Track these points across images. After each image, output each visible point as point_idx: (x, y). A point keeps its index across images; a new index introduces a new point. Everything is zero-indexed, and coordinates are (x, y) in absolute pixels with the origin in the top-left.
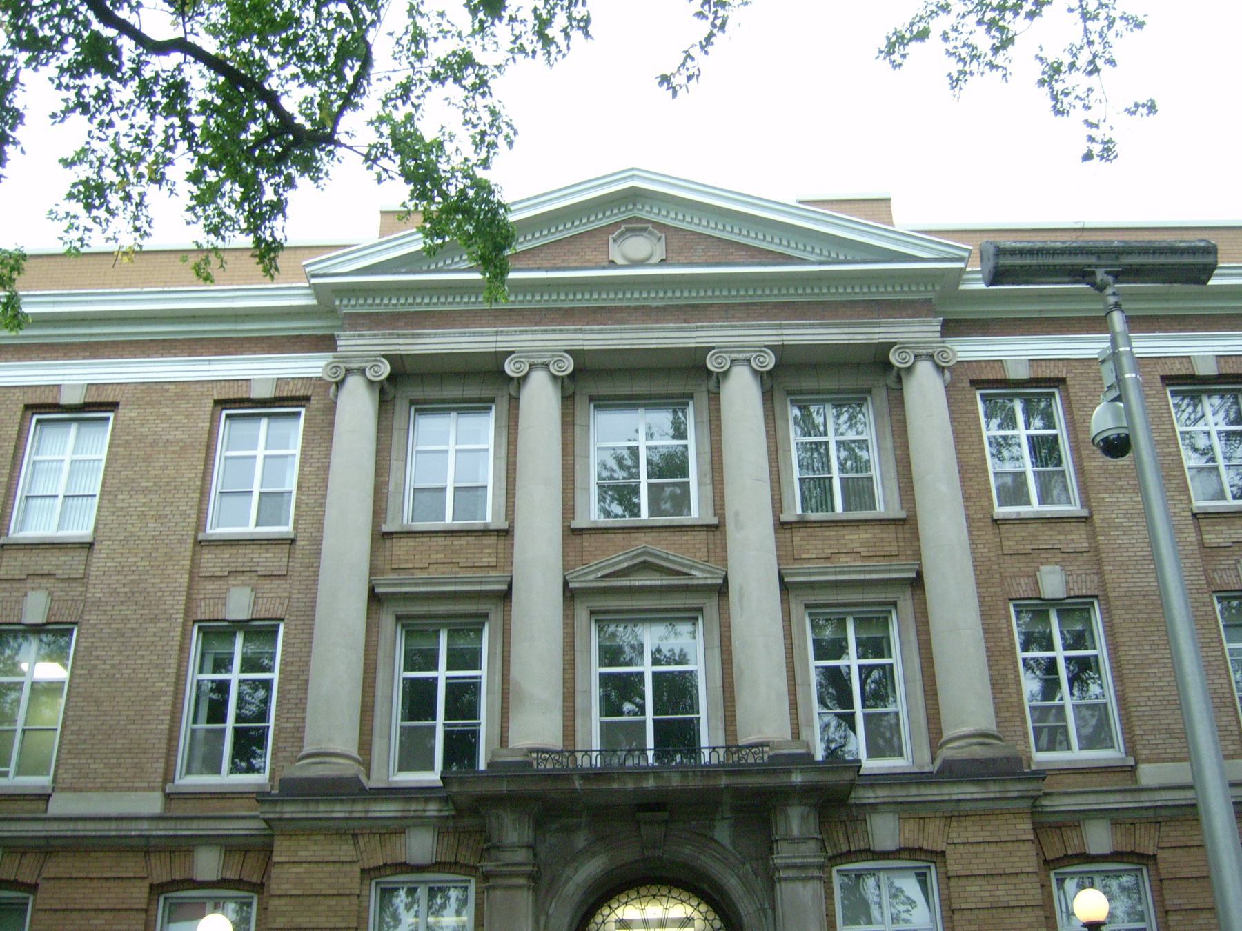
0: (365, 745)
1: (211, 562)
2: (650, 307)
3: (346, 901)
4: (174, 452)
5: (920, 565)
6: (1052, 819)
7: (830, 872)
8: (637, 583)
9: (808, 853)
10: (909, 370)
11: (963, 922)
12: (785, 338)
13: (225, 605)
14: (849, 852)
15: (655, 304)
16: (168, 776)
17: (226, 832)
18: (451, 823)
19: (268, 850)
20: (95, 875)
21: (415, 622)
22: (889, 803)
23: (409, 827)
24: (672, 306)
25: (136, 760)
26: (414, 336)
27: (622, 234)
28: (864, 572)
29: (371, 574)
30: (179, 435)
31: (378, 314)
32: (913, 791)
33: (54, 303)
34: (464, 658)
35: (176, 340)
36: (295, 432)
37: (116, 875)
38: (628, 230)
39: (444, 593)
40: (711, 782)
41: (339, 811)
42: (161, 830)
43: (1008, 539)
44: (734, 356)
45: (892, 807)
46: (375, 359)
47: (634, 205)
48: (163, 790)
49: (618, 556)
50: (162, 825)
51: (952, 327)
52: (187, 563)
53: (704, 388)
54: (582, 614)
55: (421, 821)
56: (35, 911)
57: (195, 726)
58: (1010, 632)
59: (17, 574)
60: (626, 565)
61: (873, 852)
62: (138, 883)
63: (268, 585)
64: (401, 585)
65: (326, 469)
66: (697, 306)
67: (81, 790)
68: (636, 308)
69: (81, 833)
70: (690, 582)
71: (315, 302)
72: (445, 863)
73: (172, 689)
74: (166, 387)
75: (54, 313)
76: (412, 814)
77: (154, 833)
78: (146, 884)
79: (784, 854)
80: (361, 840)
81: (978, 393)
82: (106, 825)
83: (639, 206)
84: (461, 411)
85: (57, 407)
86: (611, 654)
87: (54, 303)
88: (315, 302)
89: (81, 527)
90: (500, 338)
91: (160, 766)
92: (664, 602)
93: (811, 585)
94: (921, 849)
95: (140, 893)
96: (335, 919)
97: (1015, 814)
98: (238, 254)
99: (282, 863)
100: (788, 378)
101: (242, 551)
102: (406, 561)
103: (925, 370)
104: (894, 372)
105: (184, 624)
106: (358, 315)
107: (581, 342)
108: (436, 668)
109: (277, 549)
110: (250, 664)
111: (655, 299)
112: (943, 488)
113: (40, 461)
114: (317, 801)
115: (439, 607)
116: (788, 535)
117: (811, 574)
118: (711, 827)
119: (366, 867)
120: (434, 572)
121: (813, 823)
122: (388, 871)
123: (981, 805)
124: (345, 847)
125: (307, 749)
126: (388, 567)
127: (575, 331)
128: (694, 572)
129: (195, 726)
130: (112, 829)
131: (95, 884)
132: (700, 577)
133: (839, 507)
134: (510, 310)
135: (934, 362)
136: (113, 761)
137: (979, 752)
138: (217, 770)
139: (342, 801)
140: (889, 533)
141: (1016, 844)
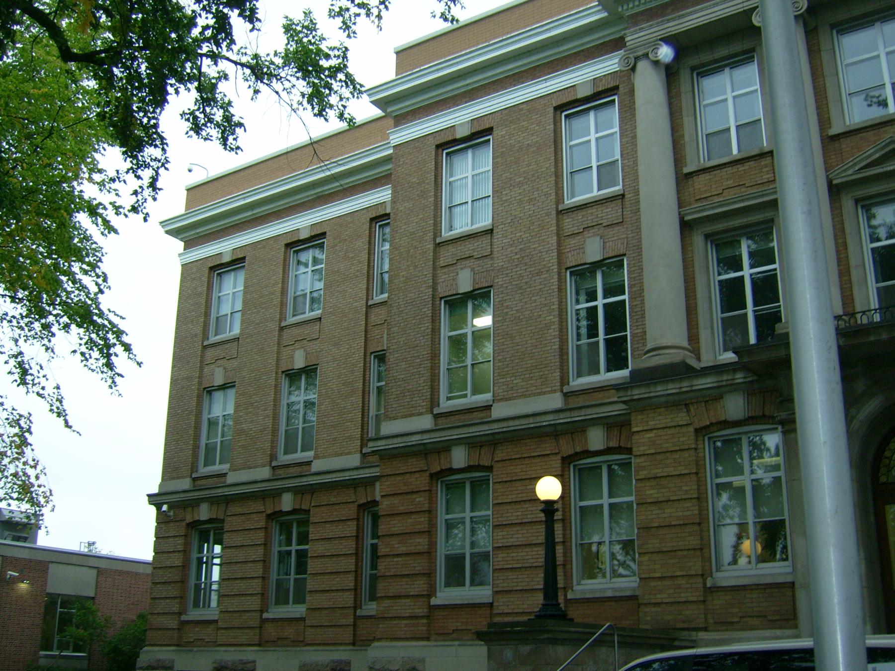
0: (693, 337)
1: (570, 224)
3: (686, 454)
4: (533, 152)
8: (889, 169)
16: (564, 381)
20: (525, 455)
21: (719, 237)
25: (541, 373)
26: (680, 17)
29: (680, 207)
30: (535, 138)
33: (438, 70)
34: (763, 256)
35: (522, 72)
36: (614, 113)
37: (539, 454)
41: (672, 388)
42: (562, 419)
48: (562, 391)
49: (871, 150)
50: (562, 415)
52: (554, 228)
54: (848, 203)
55: (734, 388)
56: (494, 483)
57: (579, 343)
59: (450, 261)
60: (877, 155)
62: (554, 457)
63: (610, 232)
64: (702, 211)
65: (634, 137)
67: (510, 399)
69: (512, 428)
71: (606, 14)
73: (557, 319)
74: (521, 107)
75: (439, 77)
76: (724, 383)
77: (558, 422)
78: (559, 457)
80: (691, 408)
82: (526, 421)
84: (733, 66)
85: (455, 142)
87: (438, 70)
88: (606, 14)
89: (485, 221)
91: (557, 374)
96: (680, 468)
99: (639, 432)
101: (590, 211)
105: (559, 273)
106: (637, 14)
109: (613, 205)
113: (455, 181)
114: (655, 384)
120: (727, 195)
124: (680, 415)
125: (649, 347)
129: (579, 343)
130: (530, 423)
131: (527, 461)
136: (527, 376)
138: (598, 372)
139: (672, 381)
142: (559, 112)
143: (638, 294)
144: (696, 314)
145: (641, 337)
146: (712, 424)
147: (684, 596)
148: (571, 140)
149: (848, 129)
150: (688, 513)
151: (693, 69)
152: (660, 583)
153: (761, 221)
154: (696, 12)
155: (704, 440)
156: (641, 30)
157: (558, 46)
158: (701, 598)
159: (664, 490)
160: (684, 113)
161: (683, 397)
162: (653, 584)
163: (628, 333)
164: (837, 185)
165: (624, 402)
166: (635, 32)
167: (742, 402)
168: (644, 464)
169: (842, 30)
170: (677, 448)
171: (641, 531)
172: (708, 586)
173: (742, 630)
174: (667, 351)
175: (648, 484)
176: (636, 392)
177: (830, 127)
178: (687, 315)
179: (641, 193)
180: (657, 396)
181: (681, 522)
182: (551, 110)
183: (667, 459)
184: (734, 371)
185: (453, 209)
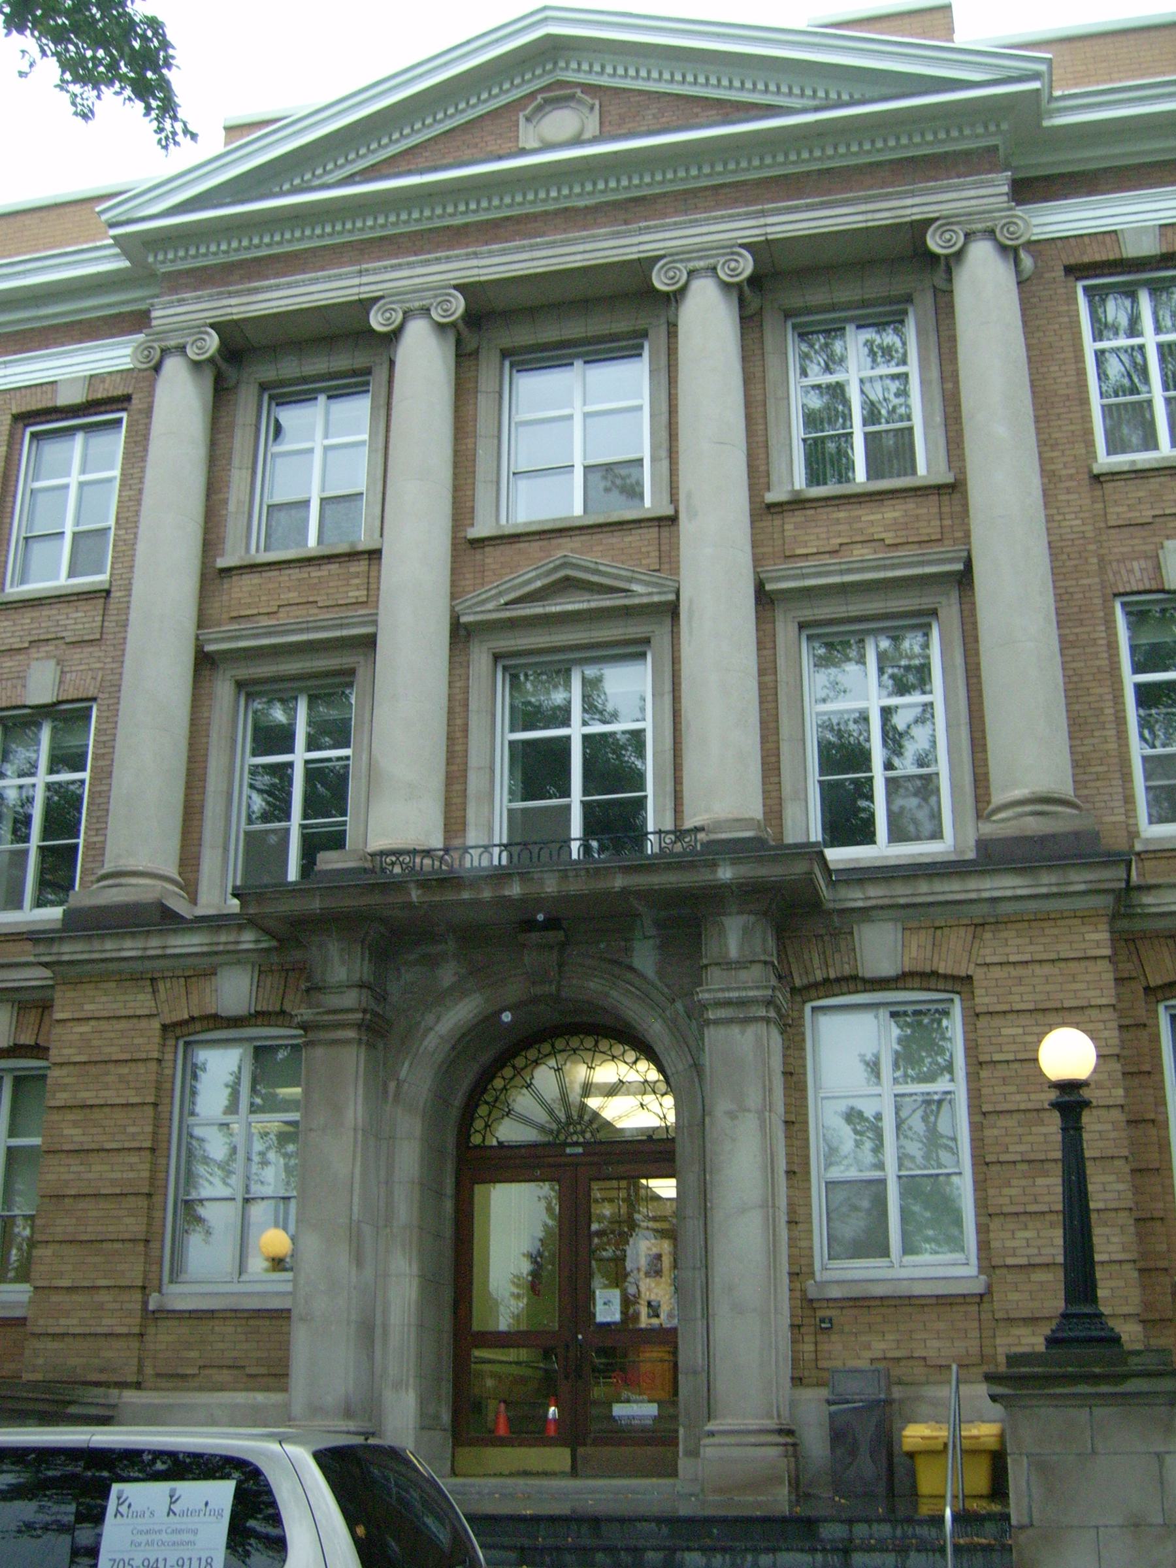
0: (189, 859)
2: (575, 210)
3: (141, 1068)
5: (969, 551)
6: (1161, 924)
7: (802, 1011)
8: (554, 609)
9: (753, 982)
10: (959, 255)
11: (993, 1082)
12: (769, 230)
13: (24, 686)
14: (826, 981)
15: (581, 203)
17: (16, 984)
18: (275, 958)
19: (45, 1007)
22: (890, 907)
23: (221, 965)
24: (607, 204)
27: (539, 108)
28: (885, 568)
29: (199, 627)
31: (205, 268)
32: (923, 887)
34: (332, 731)
36: (115, 444)
38: (547, 101)
39: (291, 644)
40: (601, 885)
41: (130, 948)
43: (1116, 503)
44: (691, 265)
45: (891, 913)
46: (198, 330)
47: (555, 64)
49: (529, 572)
51: (1029, 189)
53: (663, 320)
55: (235, 957)
58: (1113, 646)
60: (539, 584)
61: (864, 980)
63: (77, 654)
66: (643, 199)
68: (557, 213)
70: (627, 602)
71: (127, 264)
72: (269, 1014)
76: (221, 948)
79: (715, 986)
80: (161, 986)
81: (1080, 286)
83: (562, 64)
84: (334, 395)
86: (526, 717)
88: (127, 264)
90: (365, 280)
92: (595, 634)
93: (807, 593)
94: (934, 974)
95: (148, 1039)
97: (1084, 917)
98: (43, 214)
100: (783, 294)
101: (46, 612)
102: (249, 606)
103: (982, 253)
104: (943, 261)
107: (475, 271)
108: (291, 750)
110: (59, 761)
111: (580, 196)
112: (1001, 431)
115: (285, 665)
116: (777, 522)
117: (804, 576)
118: (628, 950)
119: (168, 1021)
120: (283, 618)
121: (765, 943)
122: (198, 1026)
123: (1033, 905)
124: (141, 997)
125: (108, 867)
126: (225, 616)
127: (468, 256)
128: (634, 587)
132: (642, 593)
133: (860, 473)
134: (382, 238)
135: (995, 239)
137: (1033, 826)
138: (19, 906)
139: (133, 935)
140: (927, 508)
141: (1084, 964)
142: (21, 425)
143: (103, 775)
144: (202, 820)
145: (97, 851)
146: (193, 1018)
147: (108, 1323)
148: (36, 478)
149: (500, 533)
150: (131, 1175)
151: (263, 387)
152: (67, 1298)
153: (334, 672)
154: (278, 287)
155: (176, 1046)
156: (181, 302)
157: (37, 306)
158: (136, 1330)
159: (94, 1131)
160: (236, 462)
161: (148, 964)
162: (55, 1298)
163: (81, 841)
164: (467, 626)
165: (46, 965)
166: (170, 304)
167: (247, 981)
168: (67, 1081)
169: (523, 362)
170: (127, 1056)
171: (47, 1200)
172: (151, 1307)
173: (200, 1389)
174: (134, 881)
175: (70, 1116)
176: (66, 948)
177: (769, 489)
178: (184, 821)
179: (134, 592)
180: (103, 960)
181: (118, 1191)
182: (8, 419)
183: (107, 1074)
184: (241, 927)
185: (30, 541)
